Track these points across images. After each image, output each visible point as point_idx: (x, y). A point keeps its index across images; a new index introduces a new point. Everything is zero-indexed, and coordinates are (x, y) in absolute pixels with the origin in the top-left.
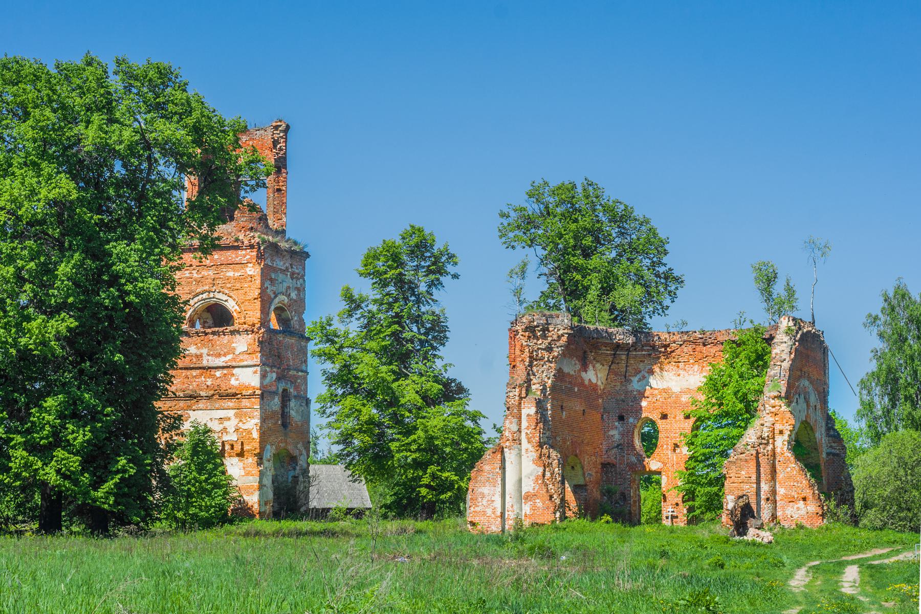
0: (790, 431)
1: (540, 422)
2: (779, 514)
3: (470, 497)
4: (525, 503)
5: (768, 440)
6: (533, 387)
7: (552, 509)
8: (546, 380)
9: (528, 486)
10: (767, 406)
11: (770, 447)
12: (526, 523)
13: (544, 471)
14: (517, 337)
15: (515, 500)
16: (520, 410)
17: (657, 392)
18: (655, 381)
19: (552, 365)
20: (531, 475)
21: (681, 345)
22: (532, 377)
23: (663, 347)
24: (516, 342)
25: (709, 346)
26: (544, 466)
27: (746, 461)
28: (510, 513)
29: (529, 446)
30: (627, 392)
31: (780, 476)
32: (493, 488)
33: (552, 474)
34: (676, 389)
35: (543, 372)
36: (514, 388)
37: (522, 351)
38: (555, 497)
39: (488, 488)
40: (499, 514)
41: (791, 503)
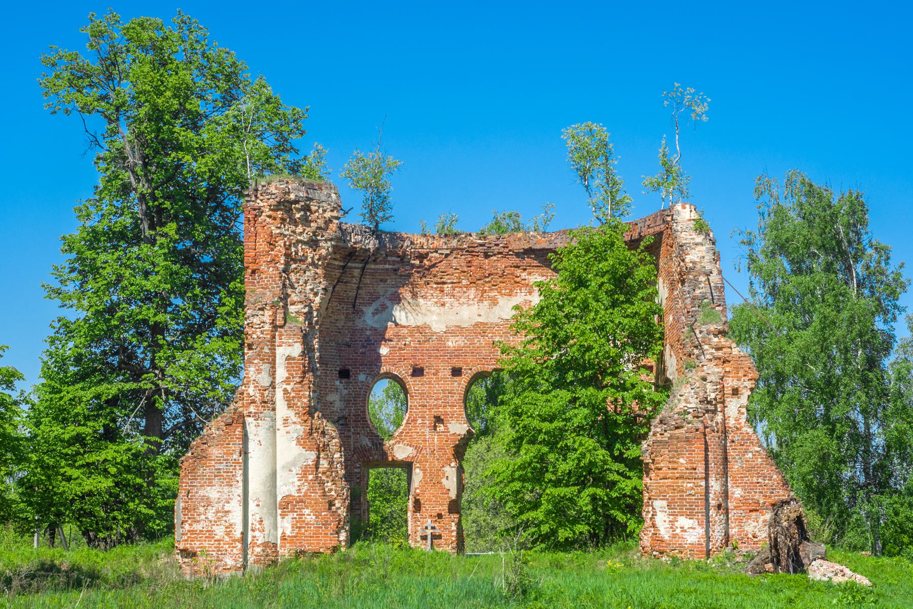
0: (752, 390)
1: (308, 371)
2: (733, 531)
3: (182, 505)
4: (283, 516)
5: (715, 405)
6: (292, 309)
7: (333, 525)
8: (311, 296)
9: (288, 485)
10: (706, 347)
11: (719, 418)
12: (285, 552)
13: (318, 457)
14: (260, 219)
15: (265, 510)
16: (273, 349)
17: (405, 331)
18: (403, 313)
19: (319, 271)
20: (294, 464)
21: (447, 255)
22: (289, 291)
23: (417, 257)
24: (259, 229)
25: (494, 258)
26: (318, 449)
27: (687, 440)
28: (257, 533)
29: (291, 414)
30: (354, 331)
31: (735, 467)
32: (226, 489)
33: (331, 463)
34: (438, 327)
35: (306, 282)
36: (262, 309)
37: (272, 244)
38: (338, 505)
39: (217, 488)
40: (238, 534)
41: (754, 514)
